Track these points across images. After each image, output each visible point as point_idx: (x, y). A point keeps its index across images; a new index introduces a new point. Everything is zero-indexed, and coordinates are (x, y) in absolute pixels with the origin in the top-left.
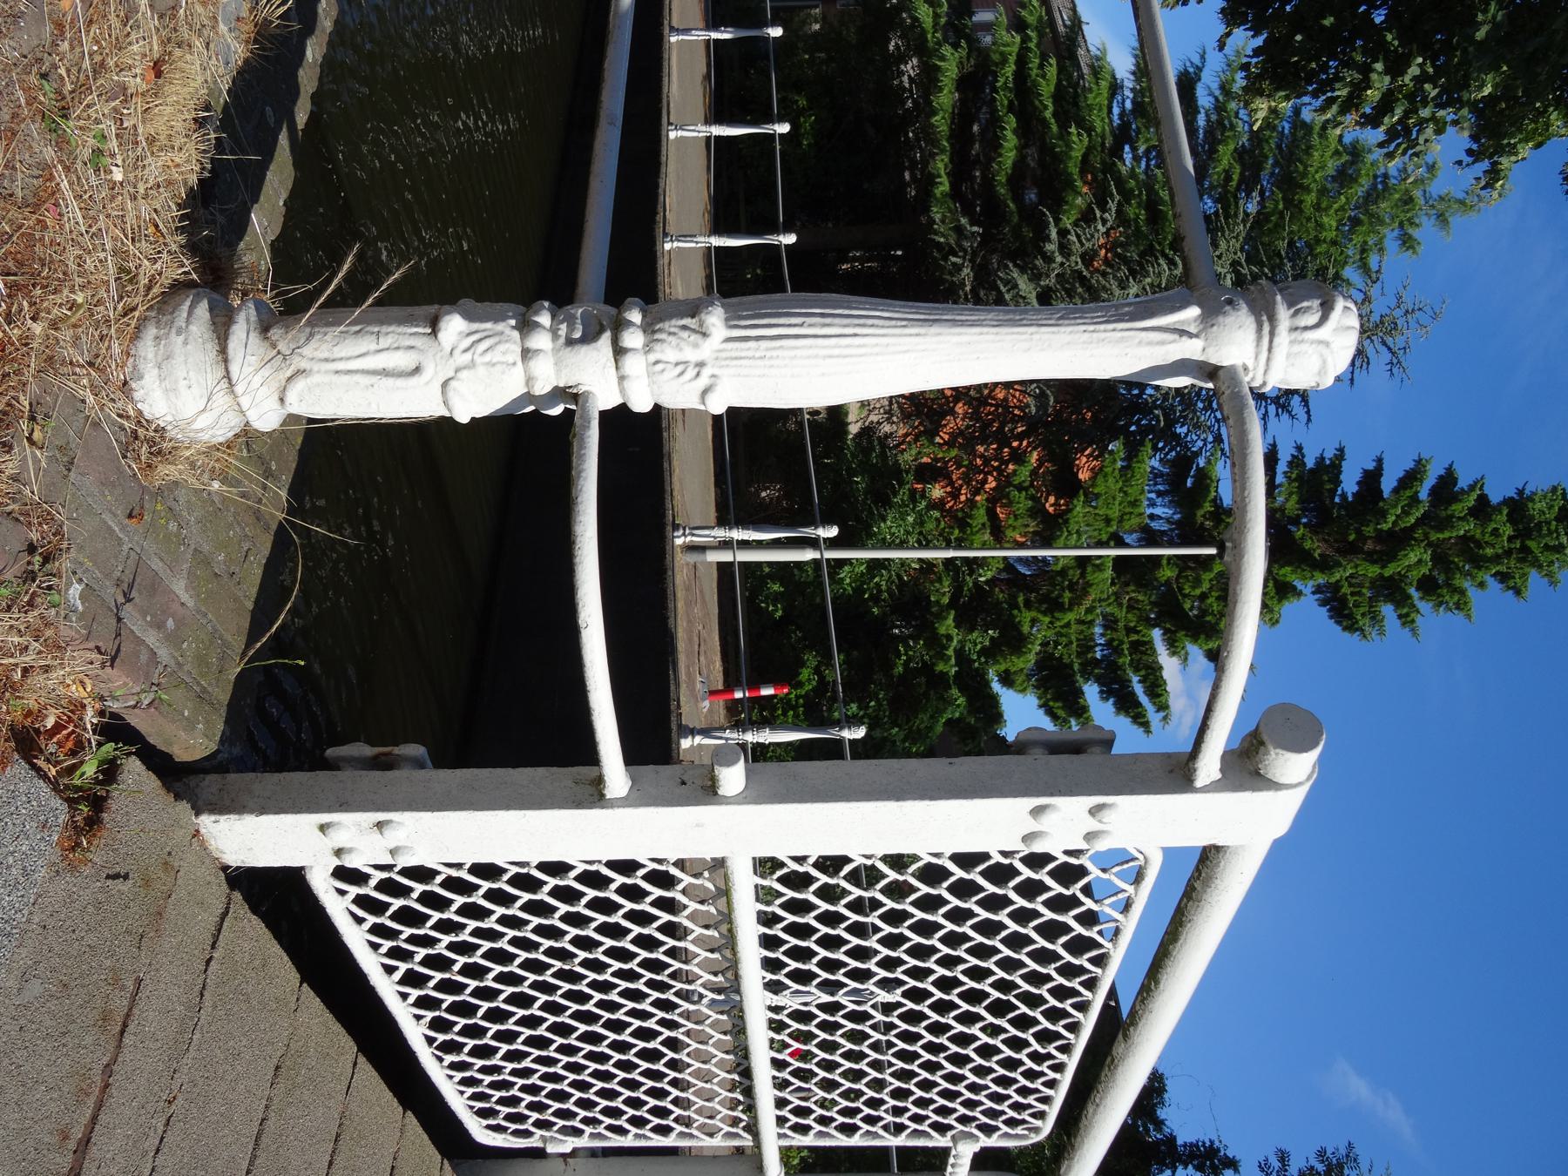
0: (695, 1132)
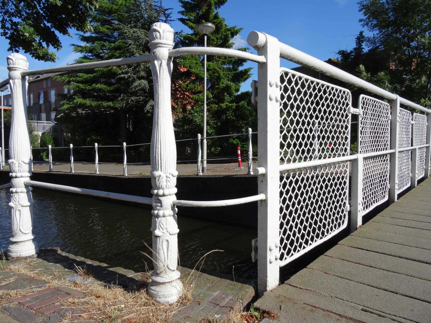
0: (346, 175)
